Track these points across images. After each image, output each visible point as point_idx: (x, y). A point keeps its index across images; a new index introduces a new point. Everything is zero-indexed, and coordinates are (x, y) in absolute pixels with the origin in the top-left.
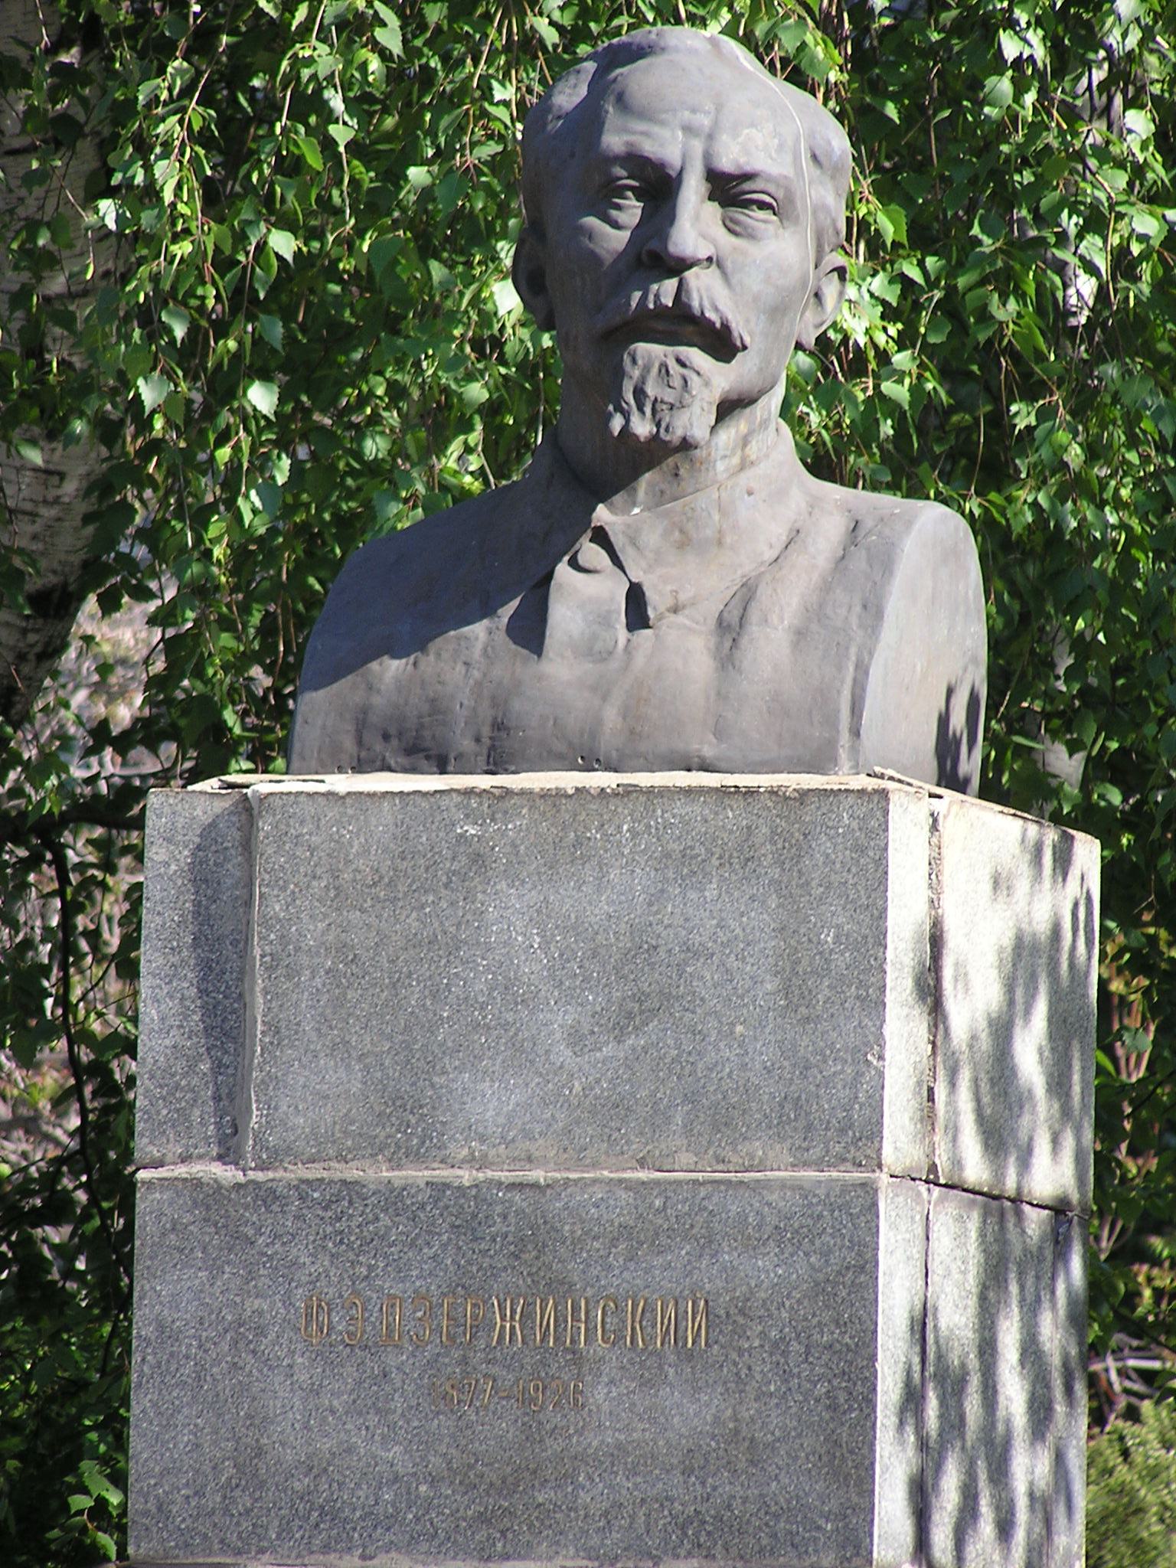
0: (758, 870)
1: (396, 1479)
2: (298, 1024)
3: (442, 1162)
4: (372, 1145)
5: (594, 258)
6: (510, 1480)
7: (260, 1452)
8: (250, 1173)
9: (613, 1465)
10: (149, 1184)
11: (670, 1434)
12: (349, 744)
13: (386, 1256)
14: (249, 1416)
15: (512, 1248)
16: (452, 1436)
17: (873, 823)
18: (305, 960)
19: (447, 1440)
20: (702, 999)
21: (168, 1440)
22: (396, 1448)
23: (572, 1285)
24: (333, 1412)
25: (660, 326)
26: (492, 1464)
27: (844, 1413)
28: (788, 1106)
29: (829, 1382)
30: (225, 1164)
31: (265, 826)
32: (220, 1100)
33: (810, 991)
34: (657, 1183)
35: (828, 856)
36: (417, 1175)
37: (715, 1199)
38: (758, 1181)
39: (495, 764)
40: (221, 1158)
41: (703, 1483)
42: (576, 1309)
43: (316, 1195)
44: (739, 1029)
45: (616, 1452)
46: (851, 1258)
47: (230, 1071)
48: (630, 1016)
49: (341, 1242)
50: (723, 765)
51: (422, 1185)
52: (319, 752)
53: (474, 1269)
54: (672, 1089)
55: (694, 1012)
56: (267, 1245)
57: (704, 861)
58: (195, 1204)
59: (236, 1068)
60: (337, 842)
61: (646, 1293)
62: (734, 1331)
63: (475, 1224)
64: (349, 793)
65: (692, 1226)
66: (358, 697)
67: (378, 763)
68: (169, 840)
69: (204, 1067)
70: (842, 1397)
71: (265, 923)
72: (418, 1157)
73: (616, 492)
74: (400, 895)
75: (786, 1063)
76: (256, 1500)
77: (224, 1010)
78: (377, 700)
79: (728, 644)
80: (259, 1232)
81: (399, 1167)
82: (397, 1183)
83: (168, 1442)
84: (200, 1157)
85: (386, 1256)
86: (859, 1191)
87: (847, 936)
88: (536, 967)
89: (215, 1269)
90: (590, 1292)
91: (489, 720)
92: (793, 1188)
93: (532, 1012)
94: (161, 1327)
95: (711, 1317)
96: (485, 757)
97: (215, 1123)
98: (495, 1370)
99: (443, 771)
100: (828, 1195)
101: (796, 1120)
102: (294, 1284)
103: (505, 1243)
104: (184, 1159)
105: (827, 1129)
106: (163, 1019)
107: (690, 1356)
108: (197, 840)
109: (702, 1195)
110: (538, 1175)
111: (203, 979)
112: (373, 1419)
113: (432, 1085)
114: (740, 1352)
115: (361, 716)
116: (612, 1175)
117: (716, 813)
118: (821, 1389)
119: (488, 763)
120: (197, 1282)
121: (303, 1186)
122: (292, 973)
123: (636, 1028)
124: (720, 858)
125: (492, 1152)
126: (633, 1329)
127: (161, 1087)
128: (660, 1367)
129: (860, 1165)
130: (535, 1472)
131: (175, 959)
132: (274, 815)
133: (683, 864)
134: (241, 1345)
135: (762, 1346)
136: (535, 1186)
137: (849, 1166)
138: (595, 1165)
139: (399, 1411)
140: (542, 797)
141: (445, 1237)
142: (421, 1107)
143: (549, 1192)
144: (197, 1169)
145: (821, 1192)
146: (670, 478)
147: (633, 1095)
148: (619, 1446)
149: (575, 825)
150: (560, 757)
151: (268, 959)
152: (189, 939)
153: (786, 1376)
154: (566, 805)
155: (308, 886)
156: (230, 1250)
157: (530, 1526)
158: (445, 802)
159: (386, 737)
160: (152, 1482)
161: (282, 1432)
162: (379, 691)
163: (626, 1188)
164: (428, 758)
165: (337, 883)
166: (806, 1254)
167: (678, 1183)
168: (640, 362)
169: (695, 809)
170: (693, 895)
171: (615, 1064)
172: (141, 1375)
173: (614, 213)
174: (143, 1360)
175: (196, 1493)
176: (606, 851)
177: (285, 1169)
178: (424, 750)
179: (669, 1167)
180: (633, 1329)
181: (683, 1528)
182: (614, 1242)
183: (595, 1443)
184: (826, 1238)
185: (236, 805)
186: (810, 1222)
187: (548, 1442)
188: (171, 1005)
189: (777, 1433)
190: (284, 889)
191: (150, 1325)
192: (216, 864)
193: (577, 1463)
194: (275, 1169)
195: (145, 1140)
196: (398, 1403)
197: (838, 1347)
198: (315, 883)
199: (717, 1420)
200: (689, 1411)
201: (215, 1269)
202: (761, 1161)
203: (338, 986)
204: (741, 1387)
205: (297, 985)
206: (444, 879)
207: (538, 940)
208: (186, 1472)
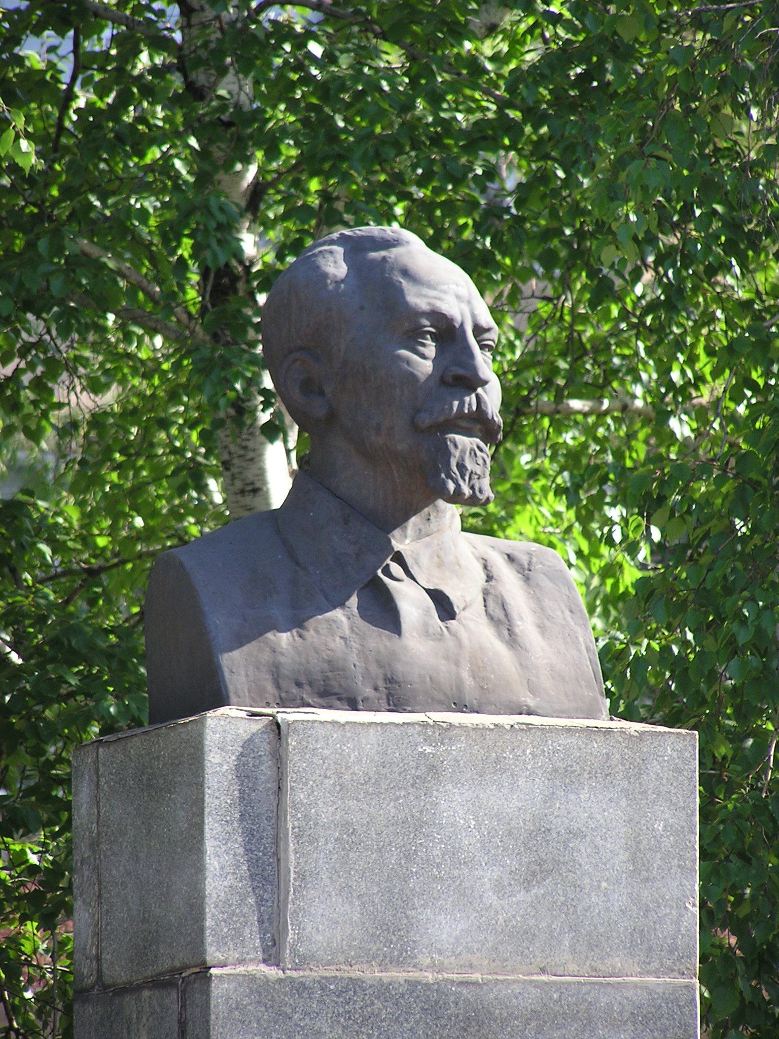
2: (318, 874)
3: (414, 966)
4: (368, 954)
5: (413, 377)
8: (288, 972)
10: (220, 977)
12: (270, 687)
13: (379, 1028)
15: (462, 1024)
25: (463, 424)
30: (268, 965)
31: (292, 742)
32: (263, 922)
33: (649, 861)
34: (555, 983)
36: (398, 975)
37: (592, 994)
38: (619, 983)
39: (395, 705)
40: (265, 961)
43: (332, 987)
44: (604, 884)
47: (269, 904)
48: (534, 874)
49: (350, 1018)
51: (402, 982)
52: (249, 693)
54: (562, 922)
55: (575, 873)
56: (300, 1020)
58: (252, 992)
63: (437, 1008)
64: (347, 723)
65: (578, 1012)
66: (266, 656)
69: (251, 901)
71: (294, 806)
72: (398, 962)
73: (395, 528)
75: (634, 907)
77: (263, 863)
78: (282, 659)
79: (506, 632)
80: (294, 1010)
82: (385, 980)
84: (251, 960)
85: (379, 1028)
86: (685, 991)
87: (672, 826)
91: (381, 677)
92: (641, 988)
93: (471, 870)
96: (385, 701)
97: (260, 938)
99: (355, 708)
101: (641, 944)
104: (241, 962)
105: (662, 950)
106: (222, 868)
109: (583, 992)
110: (477, 976)
111: (248, 843)
113: (407, 917)
119: (389, 705)
121: (323, 981)
122: (313, 840)
123: (537, 882)
125: (446, 962)
127: (223, 913)
129: (683, 974)
131: (229, 829)
133: (566, 776)
136: (475, 984)
137: (676, 974)
138: (513, 971)
140: (474, 729)
141: (418, 1016)
142: (399, 930)
143: (485, 988)
144: (251, 968)
145: (660, 991)
146: (425, 522)
147: (537, 925)
149: (496, 748)
150: (440, 702)
151: (297, 830)
152: (237, 816)
154: (490, 736)
155: (321, 784)
156: (275, 1023)
158: (411, 731)
159: (299, 684)
163: (535, 987)
164: (340, 699)
166: (651, 1031)
167: (569, 983)
170: (573, 797)
171: (525, 906)
173: (421, 348)
176: (516, 766)
177: (311, 970)
178: (335, 694)
179: (561, 973)
182: (528, 1021)
184: (664, 1021)
185: (266, 727)
186: (653, 1010)
188: (227, 859)
190: (306, 784)
192: (254, 766)
195: (214, 948)
198: (327, 781)
202: (620, 970)
203: (343, 850)
206: (411, 781)
207: (473, 823)
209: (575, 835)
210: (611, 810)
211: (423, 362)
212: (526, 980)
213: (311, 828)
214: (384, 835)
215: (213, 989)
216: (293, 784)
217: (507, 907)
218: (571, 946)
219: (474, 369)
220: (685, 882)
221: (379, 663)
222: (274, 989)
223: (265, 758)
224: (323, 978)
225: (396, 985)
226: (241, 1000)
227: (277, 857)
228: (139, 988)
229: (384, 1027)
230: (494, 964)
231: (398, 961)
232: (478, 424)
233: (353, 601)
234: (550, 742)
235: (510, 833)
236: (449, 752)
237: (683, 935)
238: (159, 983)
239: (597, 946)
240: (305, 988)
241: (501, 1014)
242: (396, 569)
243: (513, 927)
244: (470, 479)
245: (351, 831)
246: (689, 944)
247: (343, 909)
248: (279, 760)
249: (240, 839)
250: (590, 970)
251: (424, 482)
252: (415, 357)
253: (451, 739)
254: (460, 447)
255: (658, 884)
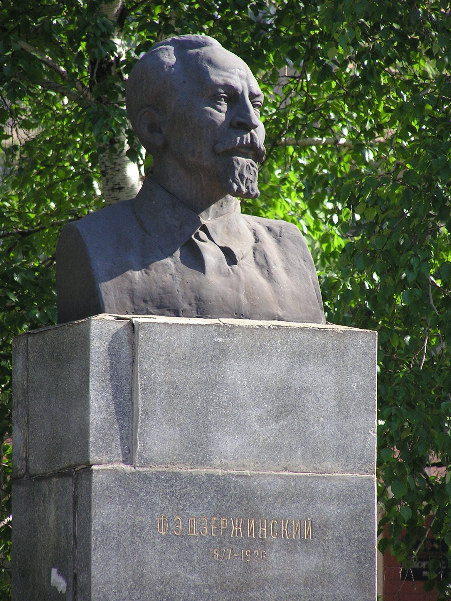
0: (328, 360)
1: (196, 587)
2: (155, 411)
3: (211, 466)
5: (213, 123)
6: (239, 588)
7: (143, 576)
8: (137, 468)
9: (278, 582)
10: (98, 471)
11: (299, 571)
12: (129, 303)
13: (190, 501)
14: (138, 562)
16: (217, 571)
19: (215, 572)
20: (308, 408)
21: (105, 569)
22: (195, 575)
23: (261, 514)
25: (243, 150)
26: (232, 582)
27: (364, 565)
29: (358, 553)
30: (125, 464)
31: (141, 335)
33: (348, 406)
34: (293, 476)
35: (354, 356)
36: (202, 471)
38: (330, 477)
39: (201, 314)
40: (124, 462)
41: (312, 590)
42: (262, 523)
43: (163, 477)
44: (322, 419)
45: (279, 578)
46: (365, 506)
48: (281, 413)
49: (173, 496)
50: (285, 318)
52: (116, 306)
53: (224, 507)
55: (305, 412)
56: (144, 496)
57: (308, 356)
59: (129, 427)
60: (169, 342)
62: (322, 533)
64: (173, 324)
65: (306, 493)
66: (126, 285)
68: (100, 338)
69: (116, 427)
70: (363, 559)
72: (202, 463)
73: (202, 211)
74: (193, 364)
75: (339, 433)
76: (142, 594)
77: (123, 405)
79: (266, 272)
80: (141, 491)
81: (194, 468)
83: (107, 571)
84: (116, 461)
85: (190, 501)
87: (361, 386)
89: (124, 505)
90: (268, 517)
91: (193, 298)
92: (343, 480)
93: (244, 410)
94: (103, 526)
95: (313, 527)
97: (121, 448)
100: (356, 483)
102: (154, 511)
103: (232, 498)
104: (110, 462)
106: (99, 408)
107: (306, 542)
108: (111, 339)
110: (247, 472)
111: (115, 393)
113: (207, 437)
114: (325, 541)
115: (131, 292)
116: (275, 473)
117: (312, 338)
118: (355, 555)
120: (117, 509)
124: (314, 355)
125: (229, 463)
126: (284, 531)
127: (99, 433)
129: (367, 472)
130: (248, 585)
132: (145, 331)
133: (300, 356)
134: (135, 534)
135: (333, 539)
136: (246, 476)
138: (268, 470)
139: (196, 561)
140: (247, 328)
141: (212, 495)
143: (252, 478)
144: (116, 466)
145: (354, 481)
148: (280, 576)
150: (227, 313)
151: (143, 386)
152: (109, 377)
153: (342, 550)
155: (158, 359)
156: (130, 498)
158: (210, 329)
159: (145, 301)
160: (101, 587)
161: (151, 568)
162: (136, 283)
164: (169, 310)
165: (169, 358)
167: (301, 477)
168: (241, 164)
169: (304, 336)
170: (304, 368)
171: (276, 431)
172: (96, 545)
173: (219, 106)
174: (97, 539)
175: (118, 591)
176: (271, 350)
177: (151, 467)
178: (166, 307)
180: (284, 531)
182: (276, 499)
183: (271, 574)
189: (339, 572)
190: (149, 359)
191: (99, 525)
192: (119, 348)
193: (264, 582)
194: (147, 467)
196: (196, 557)
197: (361, 540)
199: (316, 566)
200: (307, 563)
201: (124, 505)
202: (330, 469)
204: (325, 554)
205: (154, 397)
206: (210, 358)
207: (246, 383)
208: (115, 583)
211: (220, 114)
219: (249, 119)
227: (132, 402)
228: (50, 477)
232: (251, 150)
233: (178, 253)
238: (62, 474)
242: (202, 235)
248: (133, 345)
251: (220, 184)
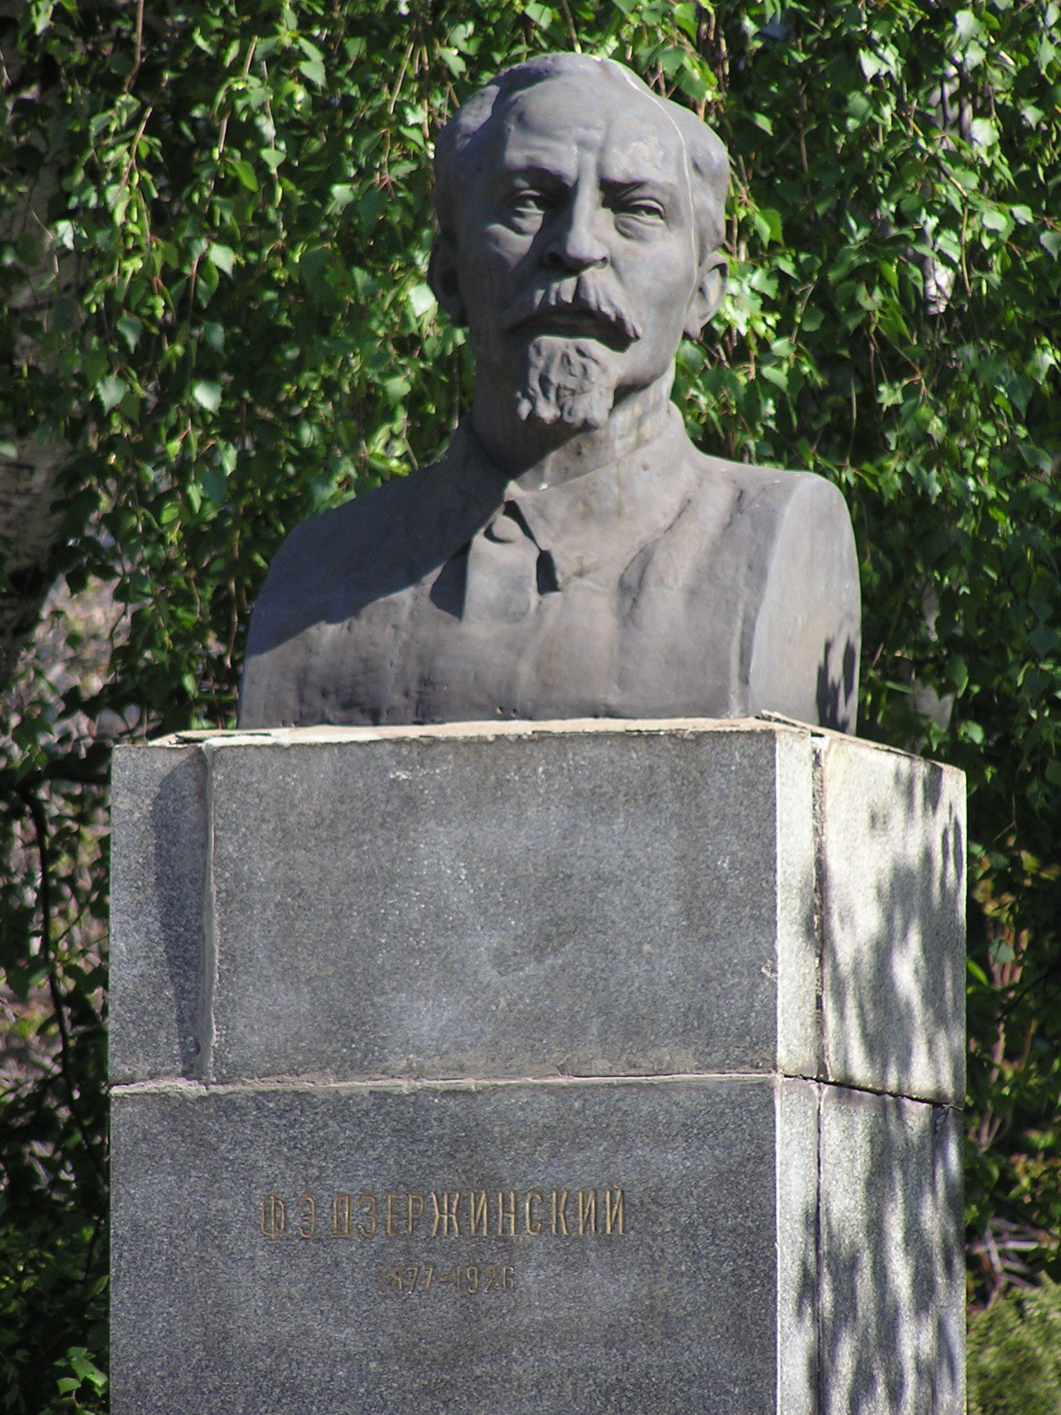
1: (349, 1357)
3: (383, 1073)
8: (212, 1087)
10: (122, 1099)
14: (216, 1304)
17: (762, 761)
18: (256, 895)
24: (291, 1299)
25: (561, 320)
28: (691, 1016)
31: (218, 776)
34: (576, 1087)
36: (361, 1085)
37: (628, 1101)
40: (185, 1074)
42: (506, 1201)
43: (271, 1105)
44: (647, 947)
47: (192, 996)
48: (549, 938)
51: (366, 1095)
55: (605, 934)
56: (229, 1151)
61: (568, 1186)
64: (293, 745)
65: (608, 1125)
67: (318, 718)
69: (168, 993)
70: (746, 1274)
71: (220, 863)
72: (361, 1069)
75: (689, 977)
82: (343, 1093)
84: (167, 1074)
88: (463, 897)
89: (182, 1174)
90: (518, 1186)
92: (698, 1089)
93: (461, 937)
98: (434, 1258)
99: (376, 723)
101: (699, 1027)
104: (153, 1076)
105: (727, 1035)
106: (130, 951)
110: (470, 1083)
112: (327, 1305)
113: (373, 1004)
114: (654, 1236)
118: (727, 1268)
119: (417, 715)
121: (260, 1098)
122: (245, 907)
125: (428, 1064)
127: (130, 1012)
128: (583, 1252)
129: (757, 1067)
131: (140, 897)
134: (208, 1240)
136: (466, 1092)
141: (387, 1140)
142: (364, 1024)
143: (479, 1097)
144: (164, 1084)
148: (547, 1323)
151: (223, 895)
152: (152, 879)
153: (696, 1257)
157: (470, 1396)
158: (379, 750)
159: (325, 694)
164: (362, 711)
166: (711, 1148)
167: (595, 1087)
170: (602, 829)
173: (518, 220)
181: (606, 1395)
182: (539, 1141)
184: (729, 1133)
187: (484, 1321)
188: (137, 939)
190: (236, 832)
195: (117, 1060)
198: (264, 826)
199: (634, 1299)
201: (182, 1174)
202: (669, 1065)
203: (286, 918)
206: (380, 820)
207: (464, 871)
209: (607, 882)
210: (656, 845)
212: (535, 1085)
213: (242, 891)
214: (342, 896)
215: (111, 1114)
216: (218, 833)
217: (510, 985)
218: (600, 1035)
220: (760, 938)
221: (421, 660)
222: (194, 1111)
223: (190, 800)
224: (259, 1093)
225: (358, 1099)
226: (150, 1128)
229: (341, 1156)
230: (494, 1065)
231: (361, 1066)
234: (570, 755)
235: (516, 883)
236: (431, 777)
237: (757, 1013)
239: (637, 1033)
240: (236, 1109)
241: (501, 1133)
243: (520, 1012)
244: (558, 397)
245: (298, 891)
246: (765, 1024)
247: (286, 998)
249: (154, 911)
250: (626, 1067)
252: (512, 234)
253: (433, 759)
254: (544, 353)
255: (723, 943)
